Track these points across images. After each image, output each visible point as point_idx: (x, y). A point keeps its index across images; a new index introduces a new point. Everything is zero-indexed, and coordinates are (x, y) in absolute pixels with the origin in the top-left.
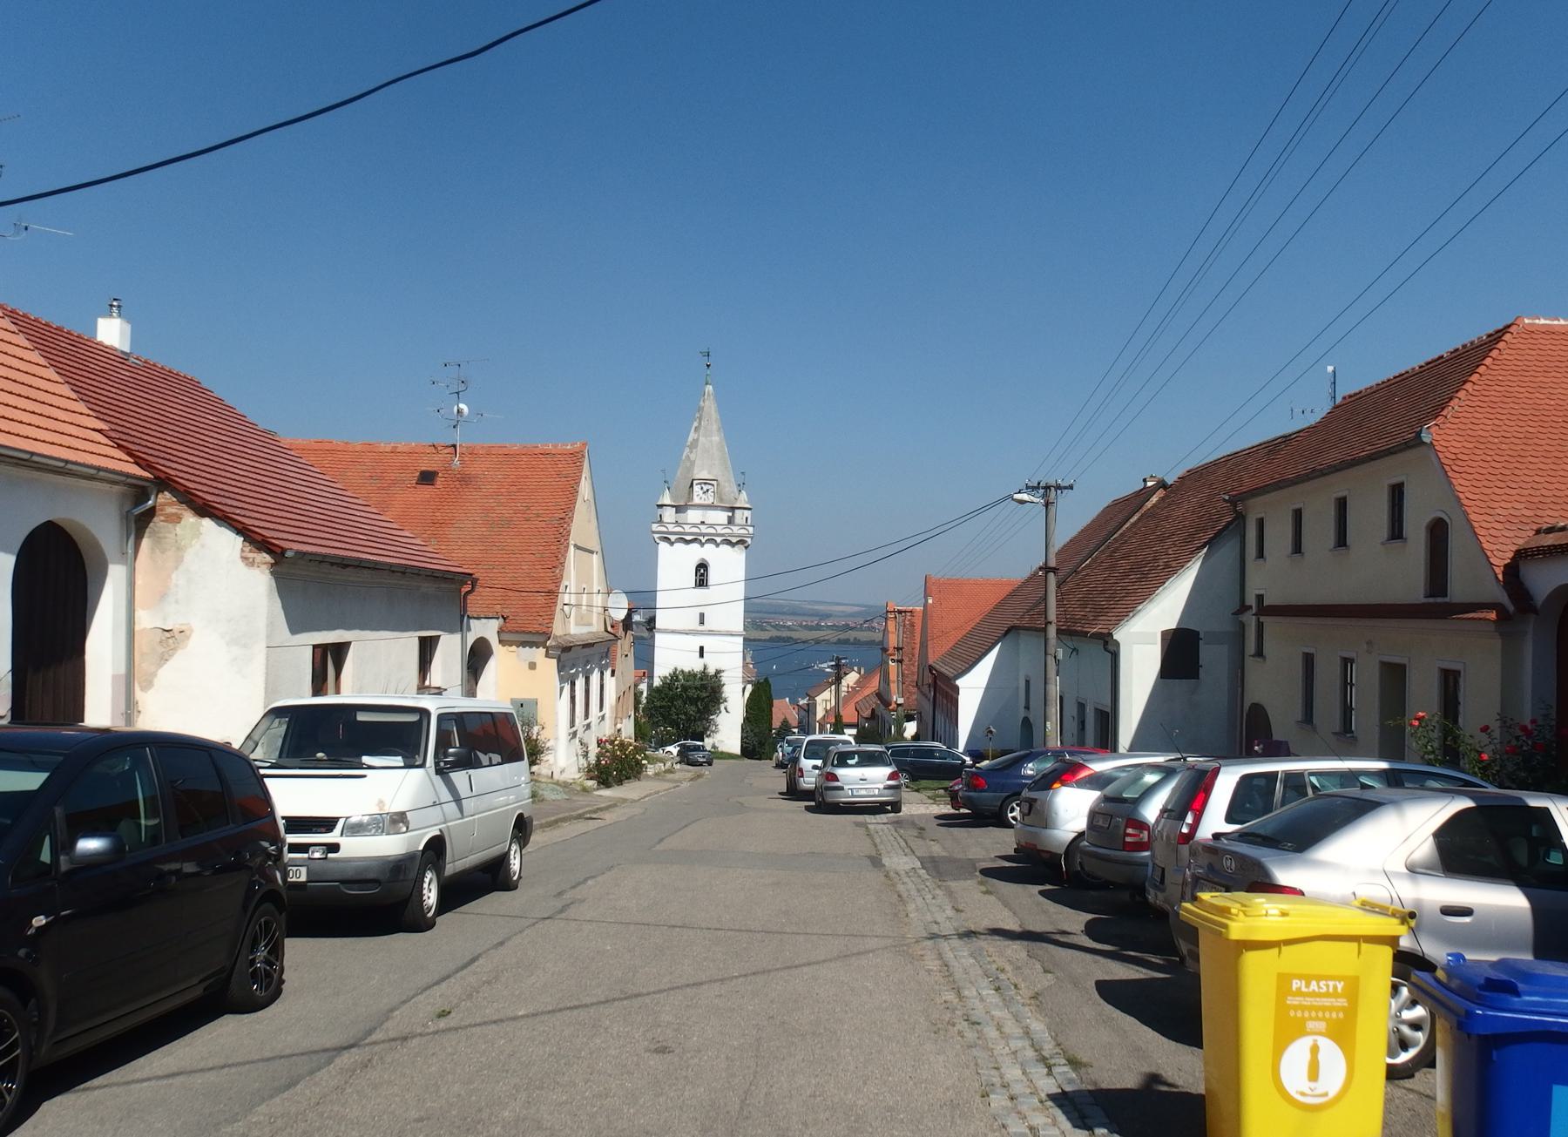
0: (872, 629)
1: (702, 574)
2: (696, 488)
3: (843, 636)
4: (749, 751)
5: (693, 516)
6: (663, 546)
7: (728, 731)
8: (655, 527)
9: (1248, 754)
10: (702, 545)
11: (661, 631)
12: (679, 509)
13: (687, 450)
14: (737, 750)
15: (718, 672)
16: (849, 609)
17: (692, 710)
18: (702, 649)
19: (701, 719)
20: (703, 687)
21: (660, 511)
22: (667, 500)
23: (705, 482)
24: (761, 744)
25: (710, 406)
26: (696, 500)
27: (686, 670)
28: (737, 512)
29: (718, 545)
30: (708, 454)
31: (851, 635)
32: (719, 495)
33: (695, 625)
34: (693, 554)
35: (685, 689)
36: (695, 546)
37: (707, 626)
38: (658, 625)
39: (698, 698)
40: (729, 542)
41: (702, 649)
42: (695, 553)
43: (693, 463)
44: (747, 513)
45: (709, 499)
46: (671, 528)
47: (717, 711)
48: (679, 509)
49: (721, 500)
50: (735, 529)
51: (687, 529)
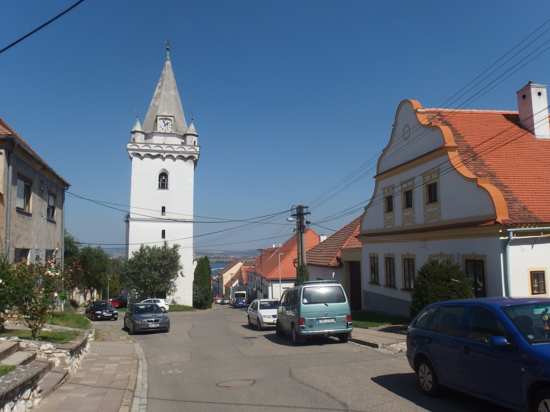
0: (227, 258)
1: (163, 180)
2: (160, 123)
3: (218, 260)
4: (201, 302)
5: (157, 139)
6: (135, 160)
7: (183, 290)
8: (129, 146)
9: (257, 308)
10: (164, 159)
11: (134, 220)
12: (148, 136)
13: (153, 100)
14: (190, 303)
15: (176, 247)
16: (219, 252)
17: (156, 275)
18: (163, 232)
19: (163, 282)
20: (164, 258)
21: (133, 136)
22: (138, 127)
23: (165, 118)
24: (206, 298)
25: (168, 72)
26: (159, 130)
27: (151, 246)
28: (188, 137)
29: (174, 159)
30: (167, 98)
31: (221, 260)
32: (175, 126)
33: (159, 215)
34: (158, 166)
35: (150, 260)
36: (159, 160)
37: (167, 216)
38: (132, 216)
39: (161, 266)
40: (182, 158)
41: (163, 232)
42: (158, 165)
43: (157, 107)
44: (195, 139)
45: (169, 130)
46: (141, 146)
47: (175, 276)
48: (148, 136)
49: (177, 130)
50: (187, 148)
51: (153, 147)
